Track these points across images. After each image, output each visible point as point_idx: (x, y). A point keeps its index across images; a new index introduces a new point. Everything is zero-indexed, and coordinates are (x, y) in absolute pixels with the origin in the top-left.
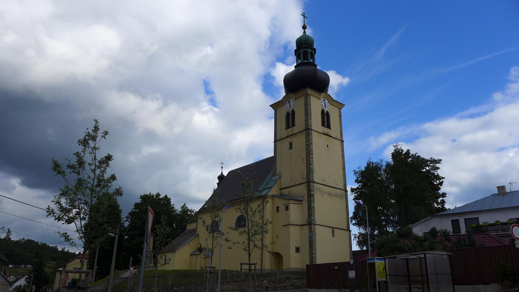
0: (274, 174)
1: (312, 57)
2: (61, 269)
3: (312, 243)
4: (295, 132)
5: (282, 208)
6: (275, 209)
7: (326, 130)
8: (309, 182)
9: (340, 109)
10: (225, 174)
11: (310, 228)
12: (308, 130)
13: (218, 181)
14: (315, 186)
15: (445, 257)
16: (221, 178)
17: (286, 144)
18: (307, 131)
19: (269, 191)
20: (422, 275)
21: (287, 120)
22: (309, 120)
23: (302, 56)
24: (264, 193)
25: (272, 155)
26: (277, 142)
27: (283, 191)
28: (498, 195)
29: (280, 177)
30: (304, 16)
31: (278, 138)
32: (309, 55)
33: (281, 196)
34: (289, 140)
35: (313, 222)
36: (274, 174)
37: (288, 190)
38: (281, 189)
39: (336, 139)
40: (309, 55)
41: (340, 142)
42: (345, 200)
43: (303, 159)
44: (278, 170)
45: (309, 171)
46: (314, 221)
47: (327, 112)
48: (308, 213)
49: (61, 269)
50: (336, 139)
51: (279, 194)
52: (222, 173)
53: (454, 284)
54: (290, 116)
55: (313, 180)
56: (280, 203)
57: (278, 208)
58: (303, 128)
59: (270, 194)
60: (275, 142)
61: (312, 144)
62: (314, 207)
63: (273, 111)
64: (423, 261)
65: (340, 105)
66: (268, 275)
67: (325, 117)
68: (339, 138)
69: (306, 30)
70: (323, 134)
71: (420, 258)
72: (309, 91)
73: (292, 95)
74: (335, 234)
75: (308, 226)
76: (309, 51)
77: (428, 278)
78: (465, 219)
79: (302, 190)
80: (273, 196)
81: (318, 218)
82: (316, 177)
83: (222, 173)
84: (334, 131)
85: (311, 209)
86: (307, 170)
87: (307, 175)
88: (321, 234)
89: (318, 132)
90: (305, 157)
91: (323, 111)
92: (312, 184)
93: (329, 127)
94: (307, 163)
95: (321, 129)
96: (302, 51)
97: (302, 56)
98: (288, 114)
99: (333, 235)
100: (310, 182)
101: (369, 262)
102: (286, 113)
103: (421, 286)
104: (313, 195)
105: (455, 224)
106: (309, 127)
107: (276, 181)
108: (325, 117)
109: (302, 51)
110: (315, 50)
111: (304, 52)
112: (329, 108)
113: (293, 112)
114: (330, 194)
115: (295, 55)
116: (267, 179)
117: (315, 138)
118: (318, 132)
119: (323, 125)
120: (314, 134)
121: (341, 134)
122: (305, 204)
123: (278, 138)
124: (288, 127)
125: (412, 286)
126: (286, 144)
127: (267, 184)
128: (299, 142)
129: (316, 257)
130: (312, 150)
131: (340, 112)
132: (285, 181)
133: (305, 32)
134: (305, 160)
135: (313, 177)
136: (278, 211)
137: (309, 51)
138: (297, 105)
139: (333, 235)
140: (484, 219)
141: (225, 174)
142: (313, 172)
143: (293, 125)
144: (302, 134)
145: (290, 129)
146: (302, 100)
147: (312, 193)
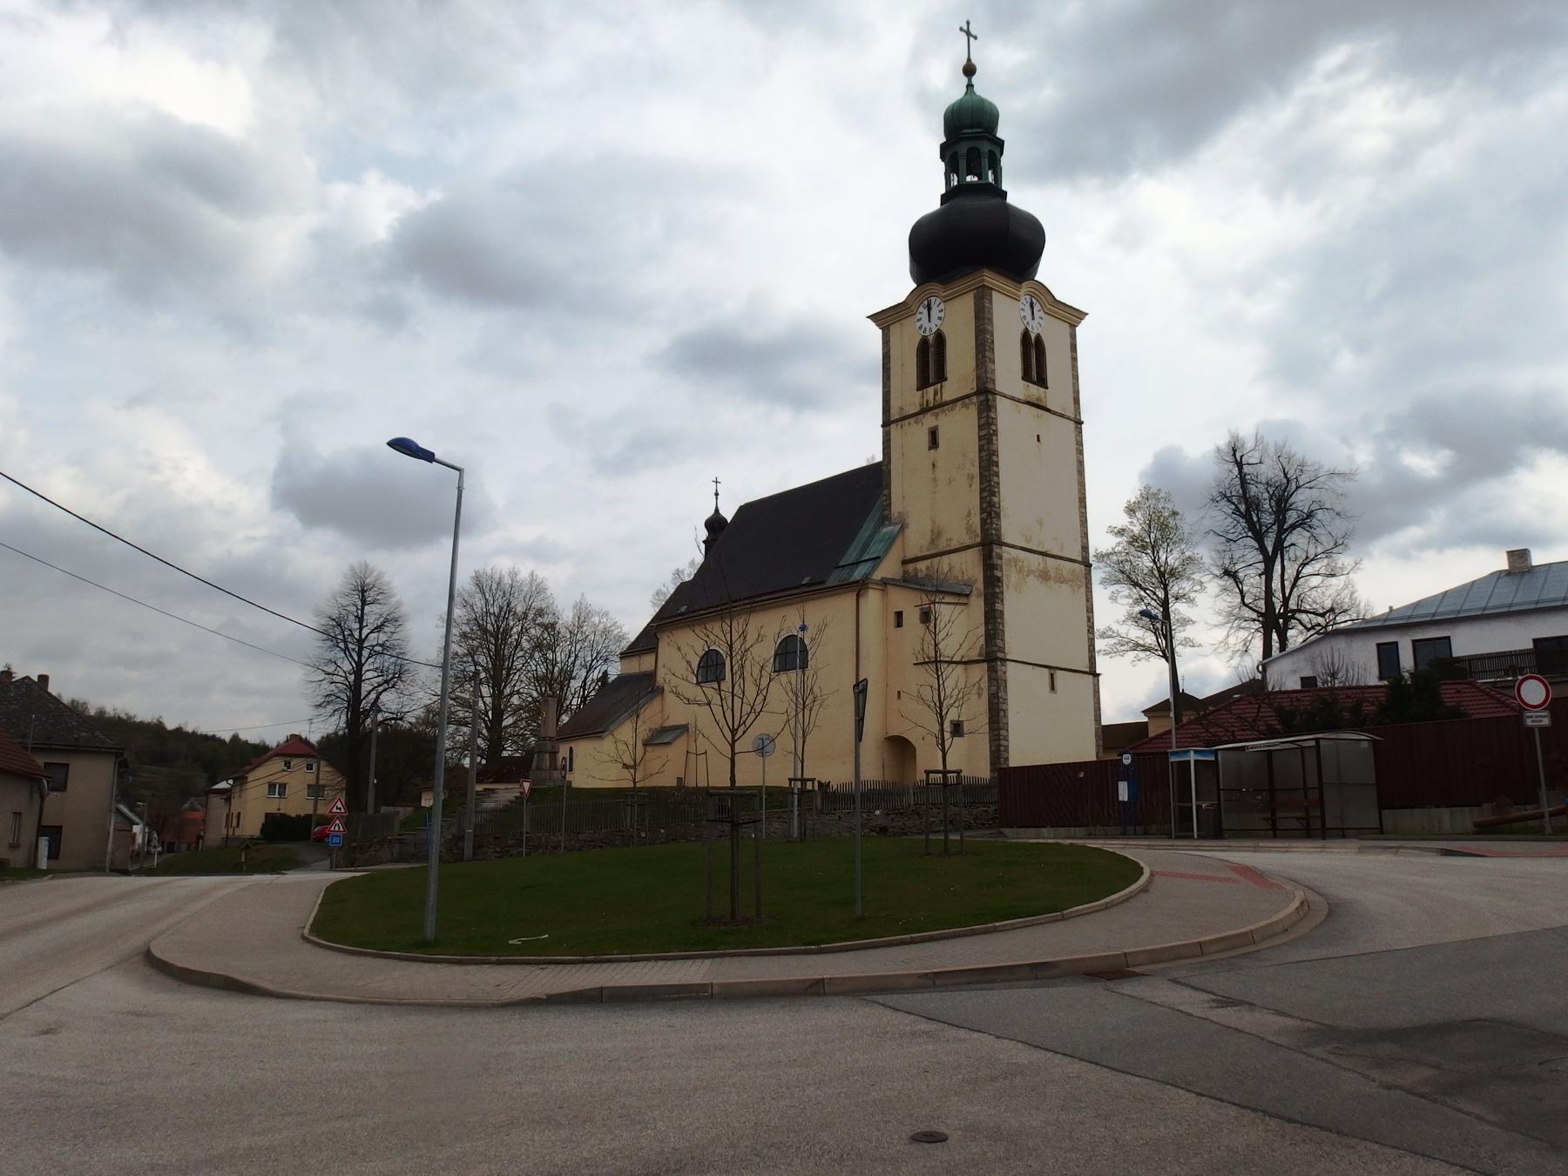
0: (885, 519)
1: (995, 166)
2: (223, 785)
3: (998, 710)
4: (947, 397)
5: (912, 617)
6: (892, 619)
7: (1035, 391)
8: (989, 542)
9: (1073, 327)
10: (728, 514)
11: (992, 671)
12: (984, 394)
13: (704, 534)
14: (1005, 556)
15: (1365, 745)
16: (715, 524)
17: (917, 434)
18: (982, 398)
19: (874, 568)
20: (1306, 789)
21: (921, 366)
22: (990, 366)
23: (963, 164)
24: (858, 574)
25: (879, 458)
26: (893, 426)
27: (910, 567)
28: (1508, 573)
29: (902, 529)
30: (968, 33)
31: (895, 415)
32: (985, 162)
33: (908, 582)
34: (929, 421)
35: (1000, 655)
36: (885, 519)
37: (928, 562)
38: (905, 562)
39: (1062, 416)
40: (985, 162)
41: (1072, 425)
42: (1083, 589)
43: (971, 477)
44: (896, 507)
45: (990, 511)
46: (1002, 650)
47: (1038, 337)
48: (987, 631)
49: (223, 785)
50: (1062, 416)
51: (899, 576)
52: (717, 510)
53: (1381, 808)
54: (931, 350)
55: (999, 536)
56: (908, 603)
57: (899, 615)
58: (971, 386)
59: (877, 576)
60: (886, 424)
61: (995, 433)
62: (1002, 612)
63: (876, 333)
64: (1311, 759)
65: (1073, 317)
66: (872, 796)
67: (1033, 353)
68: (1070, 413)
69: (974, 79)
70: (1028, 403)
71: (1303, 748)
72: (990, 278)
73: (935, 287)
74: (1058, 685)
75: (985, 665)
76: (985, 147)
77: (1321, 794)
78: (1414, 642)
79: (968, 566)
80: (885, 583)
81: (1015, 642)
82: (1010, 529)
83: (717, 510)
84: (1054, 395)
85: (995, 617)
86: (982, 510)
87: (983, 522)
88: (1021, 685)
89: (1013, 399)
90: (976, 471)
91: (1026, 335)
92: (996, 549)
93: (1042, 381)
94: (982, 491)
95: (1020, 388)
96: (963, 148)
97: (963, 164)
98: (924, 343)
99: (1053, 688)
100: (992, 543)
101: (1173, 759)
102: (918, 339)
103: (1301, 814)
104: (999, 580)
105: (1387, 654)
106: (989, 386)
107: (892, 540)
108: (1033, 353)
109: (963, 148)
110: (1000, 144)
111: (970, 150)
112: (1043, 326)
113: (940, 338)
114: (1044, 576)
115: (943, 157)
116: (864, 533)
117: (1005, 412)
118: (1013, 399)
119: (1026, 376)
120: (1001, 403)
121: (1077, 401)
122: (977, 605)
123: (895, 415)
124: (923, 383)
125: (1279, 815)
126: (917, 434)
127: (866, 546)
128: (960, 427)
129: (1007, 750)
130: (995, 453)
131: (1073, 336)
132: (915, 540)
133: (970, 86)
134: (977, 481)
135: (998, 530)
136: (899, 624)
137: (985, 147)
138: (952, 316)
139: (1053, 688)
140: (1467, 643)
141: (728, 514)
142: (998, 515)
143: (941, 377)
144: (966, 406)
145: (931, 390)
146: (966, 305)
147: (998, 573)
